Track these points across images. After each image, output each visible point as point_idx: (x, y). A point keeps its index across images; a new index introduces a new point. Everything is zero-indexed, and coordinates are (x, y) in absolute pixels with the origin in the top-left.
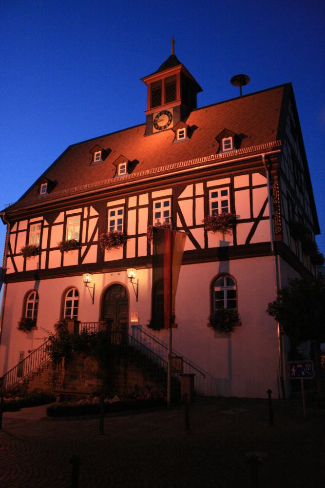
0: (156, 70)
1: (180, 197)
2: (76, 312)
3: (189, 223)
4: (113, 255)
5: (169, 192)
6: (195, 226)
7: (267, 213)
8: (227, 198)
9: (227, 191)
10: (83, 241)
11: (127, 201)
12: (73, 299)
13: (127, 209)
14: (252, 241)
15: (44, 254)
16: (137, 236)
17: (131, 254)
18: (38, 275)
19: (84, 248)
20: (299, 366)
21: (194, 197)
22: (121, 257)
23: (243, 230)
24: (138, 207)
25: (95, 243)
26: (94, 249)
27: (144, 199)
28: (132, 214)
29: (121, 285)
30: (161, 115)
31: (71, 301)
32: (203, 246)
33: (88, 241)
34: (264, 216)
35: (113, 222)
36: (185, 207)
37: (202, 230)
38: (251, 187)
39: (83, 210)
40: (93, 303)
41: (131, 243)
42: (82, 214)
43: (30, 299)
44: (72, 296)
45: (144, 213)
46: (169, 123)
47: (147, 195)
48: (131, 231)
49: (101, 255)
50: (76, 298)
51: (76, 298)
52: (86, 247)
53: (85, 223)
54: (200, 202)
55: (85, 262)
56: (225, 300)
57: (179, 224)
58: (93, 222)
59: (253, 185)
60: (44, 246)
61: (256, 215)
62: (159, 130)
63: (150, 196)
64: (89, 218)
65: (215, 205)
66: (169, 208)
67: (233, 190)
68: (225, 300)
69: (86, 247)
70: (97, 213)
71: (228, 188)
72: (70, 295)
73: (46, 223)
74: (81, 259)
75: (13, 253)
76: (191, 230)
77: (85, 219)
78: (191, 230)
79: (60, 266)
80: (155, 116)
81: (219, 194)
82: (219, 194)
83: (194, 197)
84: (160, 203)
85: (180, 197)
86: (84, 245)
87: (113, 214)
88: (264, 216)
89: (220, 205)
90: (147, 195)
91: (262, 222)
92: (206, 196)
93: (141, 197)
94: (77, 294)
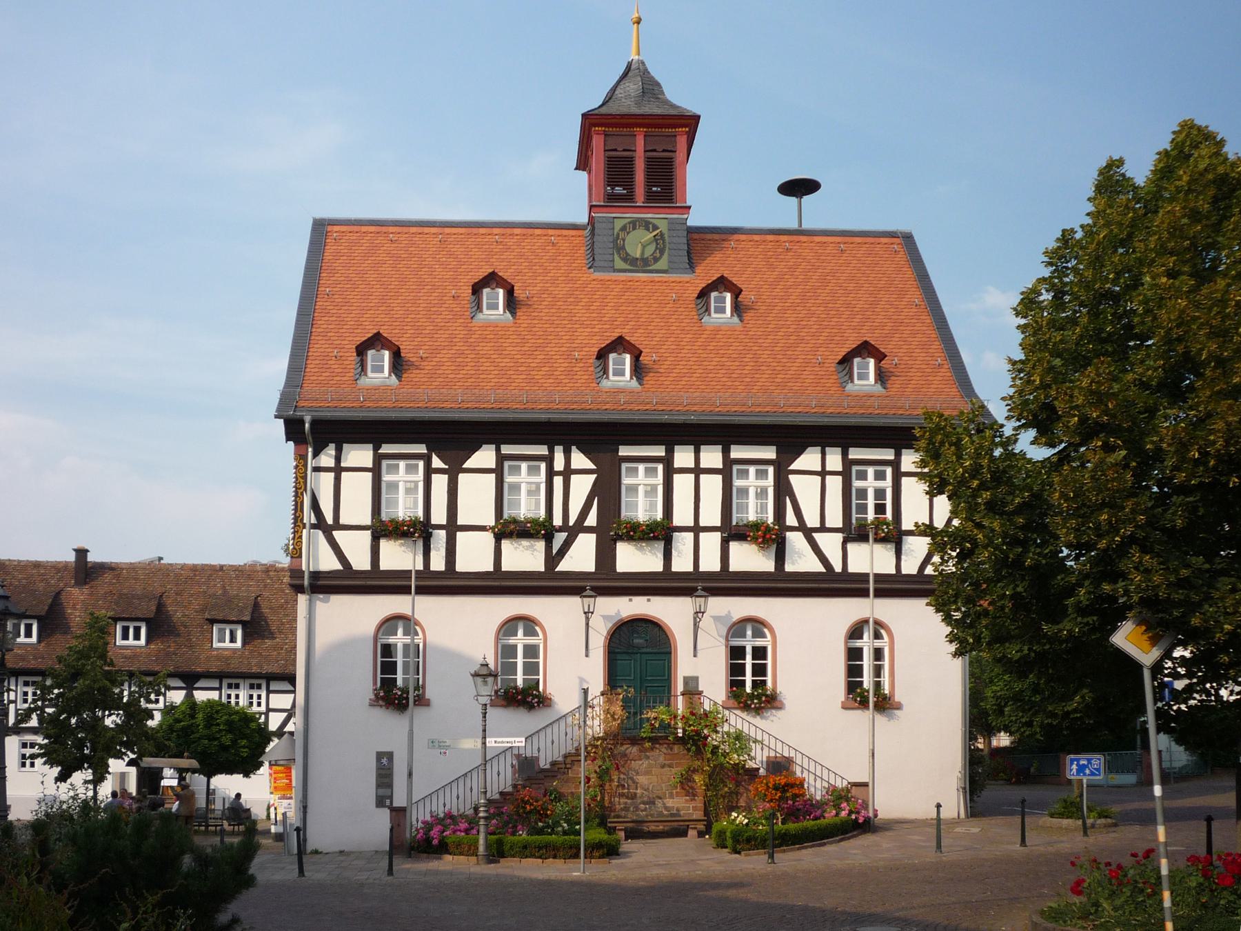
2: (759, 670)
3: (812, 521)
4: (633, 559)
6: (823, 529)
7: (591, 520)
10: (558, 521)
15: (440, 537)
16: (697, 529)
17: (682, 563)
19: (560, 538)
20: (1082, 762)
24: (697, 471)
25: (589, 530)
28: (683, 484)
30: (634, 229)
32: (838, 568)
33: (571, 524)
37: (839, 537)
39: (552, 451)
40: (587, 656)
41: (683, 542)
42: (549, 460)
46: (622, 235)
49: (605, 555)
52: (564, 535)
53: (558, 481)
55: (564, 566)
56: (520, 660)
57: (791, 520)
58: (582, 486)
60: (439, 515)
62: (631, 264)
64: (568, 473)
65: (862, 493)
67: (898, 476)
69: (564, 535)
70: (590, 465)
73: (437, 463)
74: (552, 559)
75: (330, 521)
76: (816, 536)
77: (559, 473)
78: (816, 536)
80: (618, 224)
81: (880, 484)
82: (880, 484)
85: (792, 467)
86: (560, 530)
91: (582, 537)
92: (846, 475)
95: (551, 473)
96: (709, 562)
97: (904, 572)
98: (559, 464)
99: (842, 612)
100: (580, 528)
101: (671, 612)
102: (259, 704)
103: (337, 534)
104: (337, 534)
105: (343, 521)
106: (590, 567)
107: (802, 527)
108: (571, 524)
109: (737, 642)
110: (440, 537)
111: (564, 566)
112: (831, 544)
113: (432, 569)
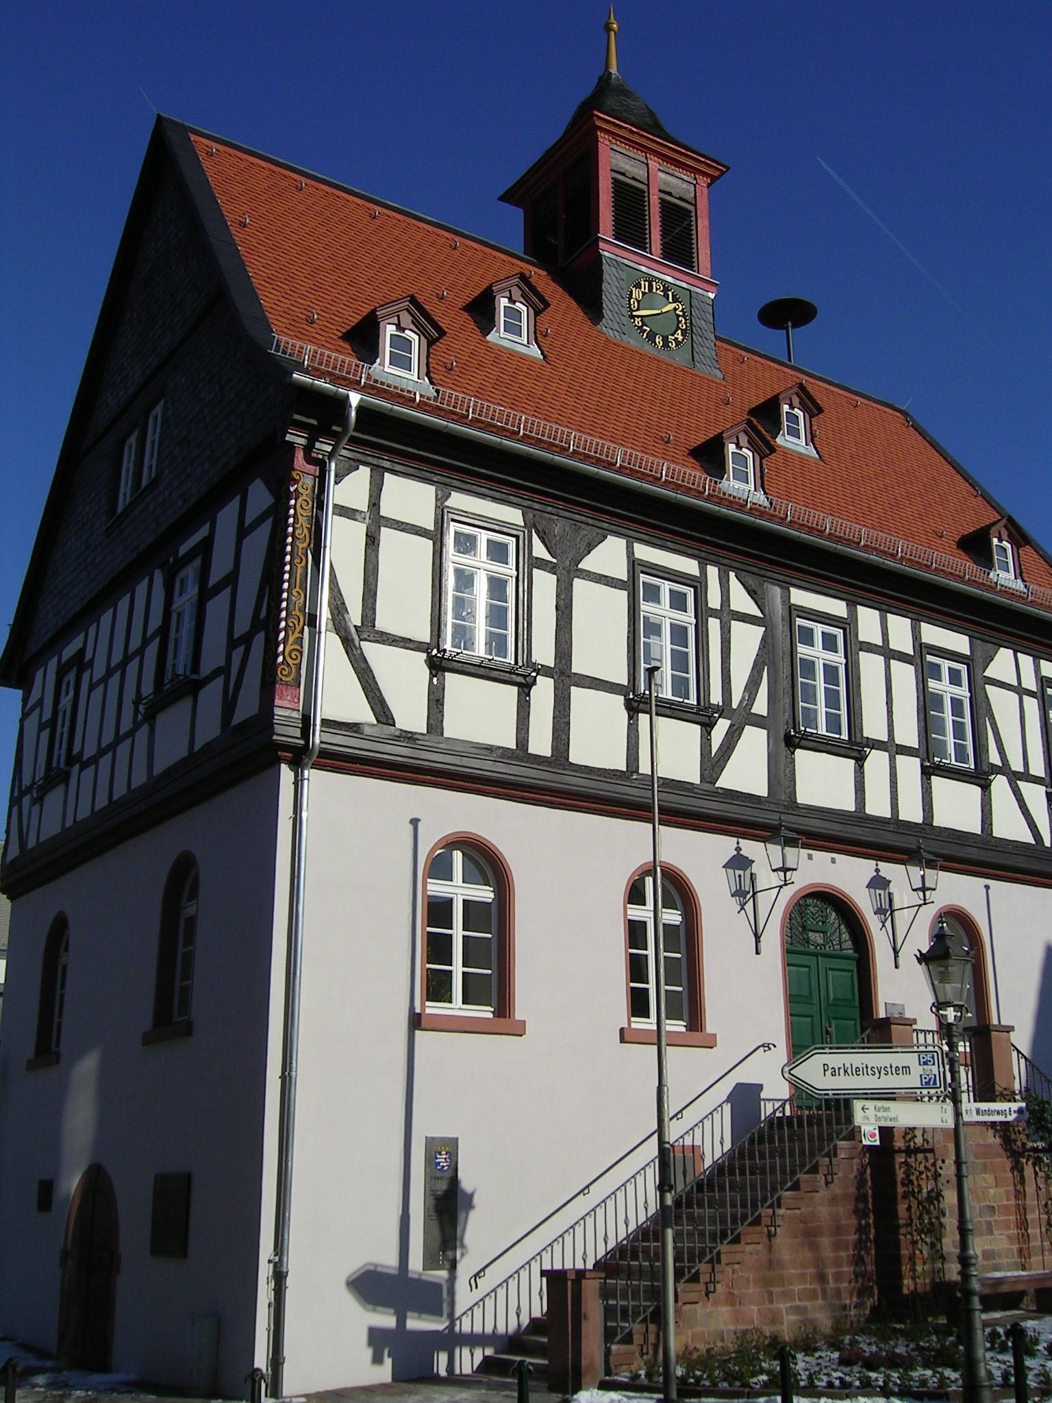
3: (1017, 765)
7: (761, 706)
15: (544, 690)
33: (735, 706)
40: (757, 953)
75: (355, 616)
81: (465, 560)
95: (703, 613)
97: (869, 811)
99: (626, 843)
101: (521, 832)
102: (906, 1069)
103: (371, 650)
104: (371, 650)
105: (382, 624)
106: (758, 786)
107: (1004, 769)
109: (437, 888)
110: (544, 690)
111: (727, 780)
113: (869, 811)
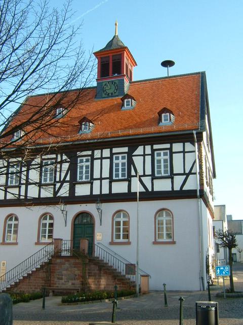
0: (12, 92)
1: (134, 154)
5: (126, 149)
6: (144, 175)
7: (68, 178)
8: (89, 164)
9: (167, 152)
11: (93, 153)
12: (13, 222)
13: (93, 159)
14: (184, 189)
15: (23, 187)
17: (96, 192)
18: (129, 197)
19: (58, 185)
21: (144, 155)
22: (88, 193)
23: (179, 180)
24: (102, 158)
25: (67, 182)
26: (66, 186)
27: (106, 153)
28: (97, 163)
29: (87, 213)
31: (46, 224)
32: (150, 190)
33: (62, 180)
34: (192, 172)
35: (81, 167)
36: (138, 161)
38: (184, 152)
39: (57, 156)
41: (96, 184)
42: (56, 158)
43: (9, 220)
44: (46, 219)
45: (106, 163)
47: (108, 150)
48: (97, 175)
50: (16, 222)
51: (16, 222)
54: (148, 159)
58: (66, 166)
59: (186, 151)
61: (187, 171)
63: (111, 151)
66: (125, 161)
67: (172, 153)
68: (122, 227)
71: (90, 158)
72: (11, 219)
74: (55, 193)
79: (108, 193)
83: (144, 155)
84: (118, 157)
85: (134, 154)
86: (58, 182)
87: (82, 161)
88: (192, 172)
89: (84, 168)
90: (108, 150)
92: (152, 155)
93: (104, 151)
94: (16, 219)
96: (106, 191)
98: (59, 160)
100: (64, 181)
108: (62, 180)
112: (147, 181)
